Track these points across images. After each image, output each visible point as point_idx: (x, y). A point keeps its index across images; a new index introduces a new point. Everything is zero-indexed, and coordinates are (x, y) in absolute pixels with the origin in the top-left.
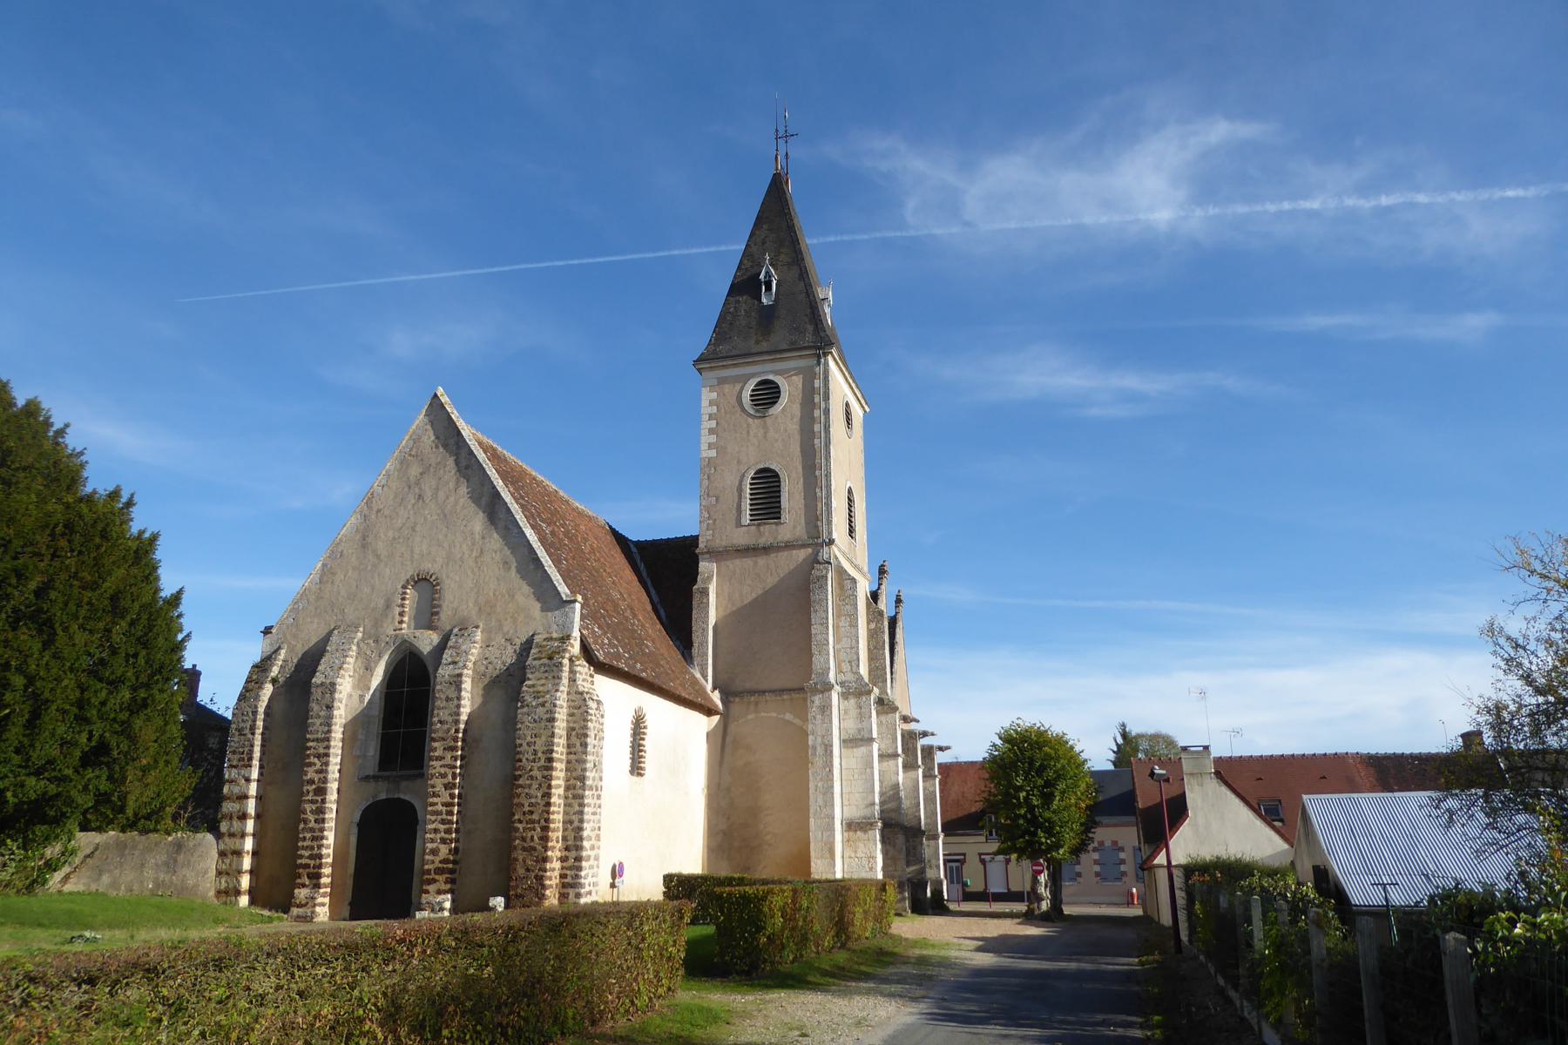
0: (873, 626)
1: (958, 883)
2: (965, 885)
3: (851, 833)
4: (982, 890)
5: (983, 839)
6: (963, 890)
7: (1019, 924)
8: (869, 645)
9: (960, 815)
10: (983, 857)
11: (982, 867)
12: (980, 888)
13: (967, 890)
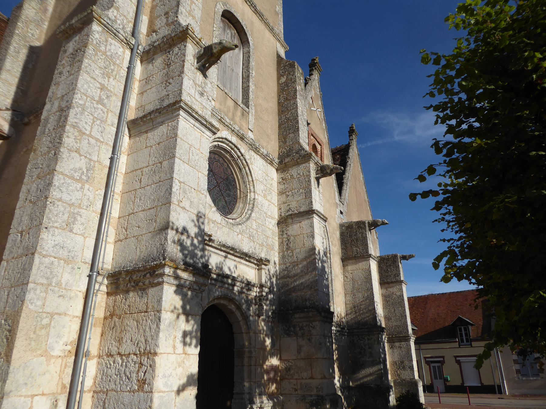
0: (283, 80)
1: (440, 378)
2: (446, 380)
3: (119, 298)
4: (460, 384)
5: (456, 345)
6: (445, 384)
7: (279, 56)
8: (279, 100)
9: (437, 328)
10: (458, 359)
11: (457, 367)
12: (458, 382)
13: (448, 384)
